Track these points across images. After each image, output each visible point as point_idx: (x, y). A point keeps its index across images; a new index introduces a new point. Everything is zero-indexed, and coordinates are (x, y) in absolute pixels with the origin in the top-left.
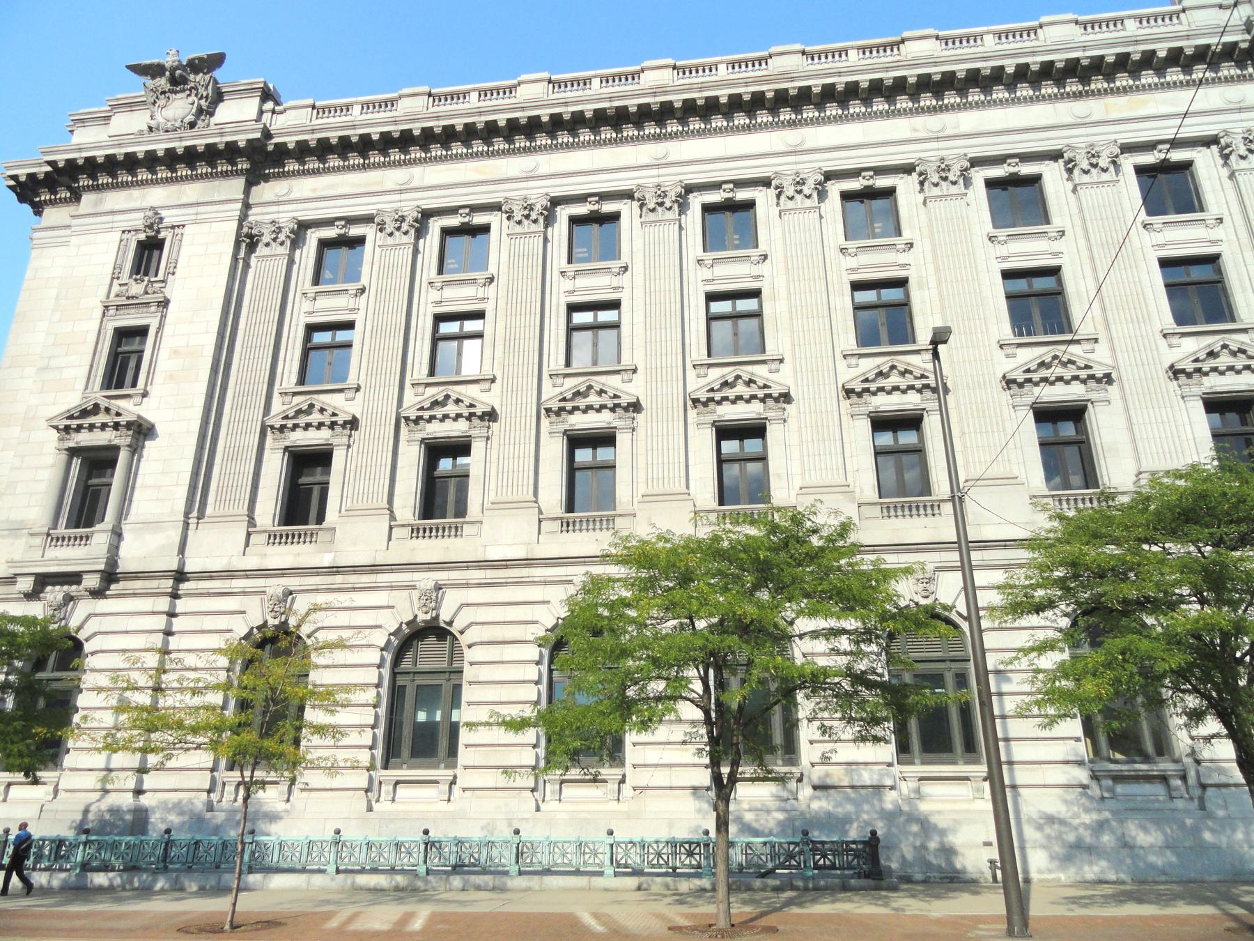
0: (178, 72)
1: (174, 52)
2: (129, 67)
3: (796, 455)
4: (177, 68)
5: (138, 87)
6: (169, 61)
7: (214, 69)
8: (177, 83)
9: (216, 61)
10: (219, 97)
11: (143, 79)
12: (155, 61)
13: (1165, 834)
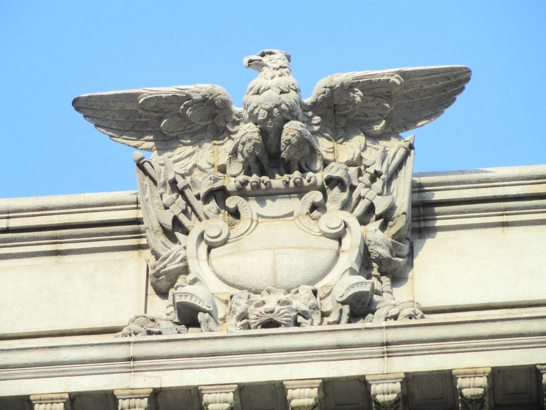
0: (292, 129)
1: (278, 59)
2: (79, 104)
3: (429, 97)
4: (289, 115)
5: (111, 175)
6: (256, 91)
7: (409, 124)
8: (274, 160)
9: (433, 93)
10: (423, 216)
11: (128, 150)
12: (198, 88)
13: (155, 150)
